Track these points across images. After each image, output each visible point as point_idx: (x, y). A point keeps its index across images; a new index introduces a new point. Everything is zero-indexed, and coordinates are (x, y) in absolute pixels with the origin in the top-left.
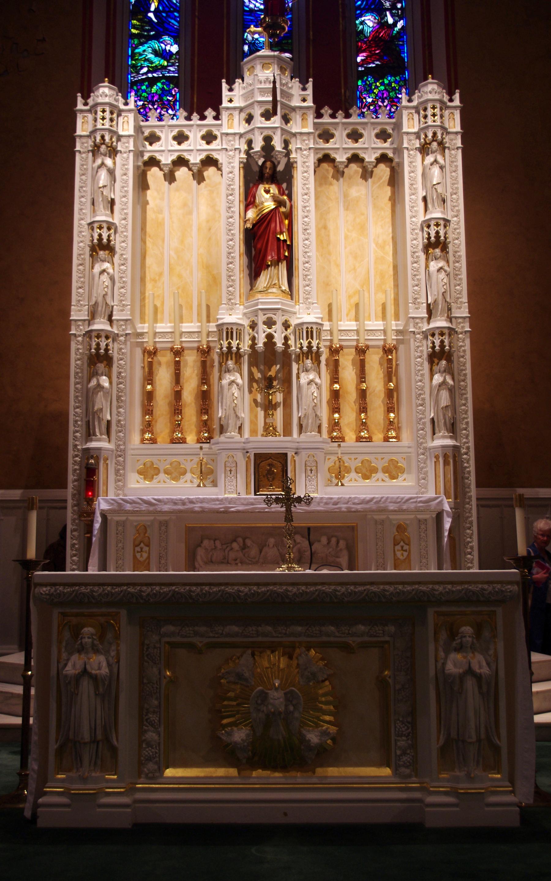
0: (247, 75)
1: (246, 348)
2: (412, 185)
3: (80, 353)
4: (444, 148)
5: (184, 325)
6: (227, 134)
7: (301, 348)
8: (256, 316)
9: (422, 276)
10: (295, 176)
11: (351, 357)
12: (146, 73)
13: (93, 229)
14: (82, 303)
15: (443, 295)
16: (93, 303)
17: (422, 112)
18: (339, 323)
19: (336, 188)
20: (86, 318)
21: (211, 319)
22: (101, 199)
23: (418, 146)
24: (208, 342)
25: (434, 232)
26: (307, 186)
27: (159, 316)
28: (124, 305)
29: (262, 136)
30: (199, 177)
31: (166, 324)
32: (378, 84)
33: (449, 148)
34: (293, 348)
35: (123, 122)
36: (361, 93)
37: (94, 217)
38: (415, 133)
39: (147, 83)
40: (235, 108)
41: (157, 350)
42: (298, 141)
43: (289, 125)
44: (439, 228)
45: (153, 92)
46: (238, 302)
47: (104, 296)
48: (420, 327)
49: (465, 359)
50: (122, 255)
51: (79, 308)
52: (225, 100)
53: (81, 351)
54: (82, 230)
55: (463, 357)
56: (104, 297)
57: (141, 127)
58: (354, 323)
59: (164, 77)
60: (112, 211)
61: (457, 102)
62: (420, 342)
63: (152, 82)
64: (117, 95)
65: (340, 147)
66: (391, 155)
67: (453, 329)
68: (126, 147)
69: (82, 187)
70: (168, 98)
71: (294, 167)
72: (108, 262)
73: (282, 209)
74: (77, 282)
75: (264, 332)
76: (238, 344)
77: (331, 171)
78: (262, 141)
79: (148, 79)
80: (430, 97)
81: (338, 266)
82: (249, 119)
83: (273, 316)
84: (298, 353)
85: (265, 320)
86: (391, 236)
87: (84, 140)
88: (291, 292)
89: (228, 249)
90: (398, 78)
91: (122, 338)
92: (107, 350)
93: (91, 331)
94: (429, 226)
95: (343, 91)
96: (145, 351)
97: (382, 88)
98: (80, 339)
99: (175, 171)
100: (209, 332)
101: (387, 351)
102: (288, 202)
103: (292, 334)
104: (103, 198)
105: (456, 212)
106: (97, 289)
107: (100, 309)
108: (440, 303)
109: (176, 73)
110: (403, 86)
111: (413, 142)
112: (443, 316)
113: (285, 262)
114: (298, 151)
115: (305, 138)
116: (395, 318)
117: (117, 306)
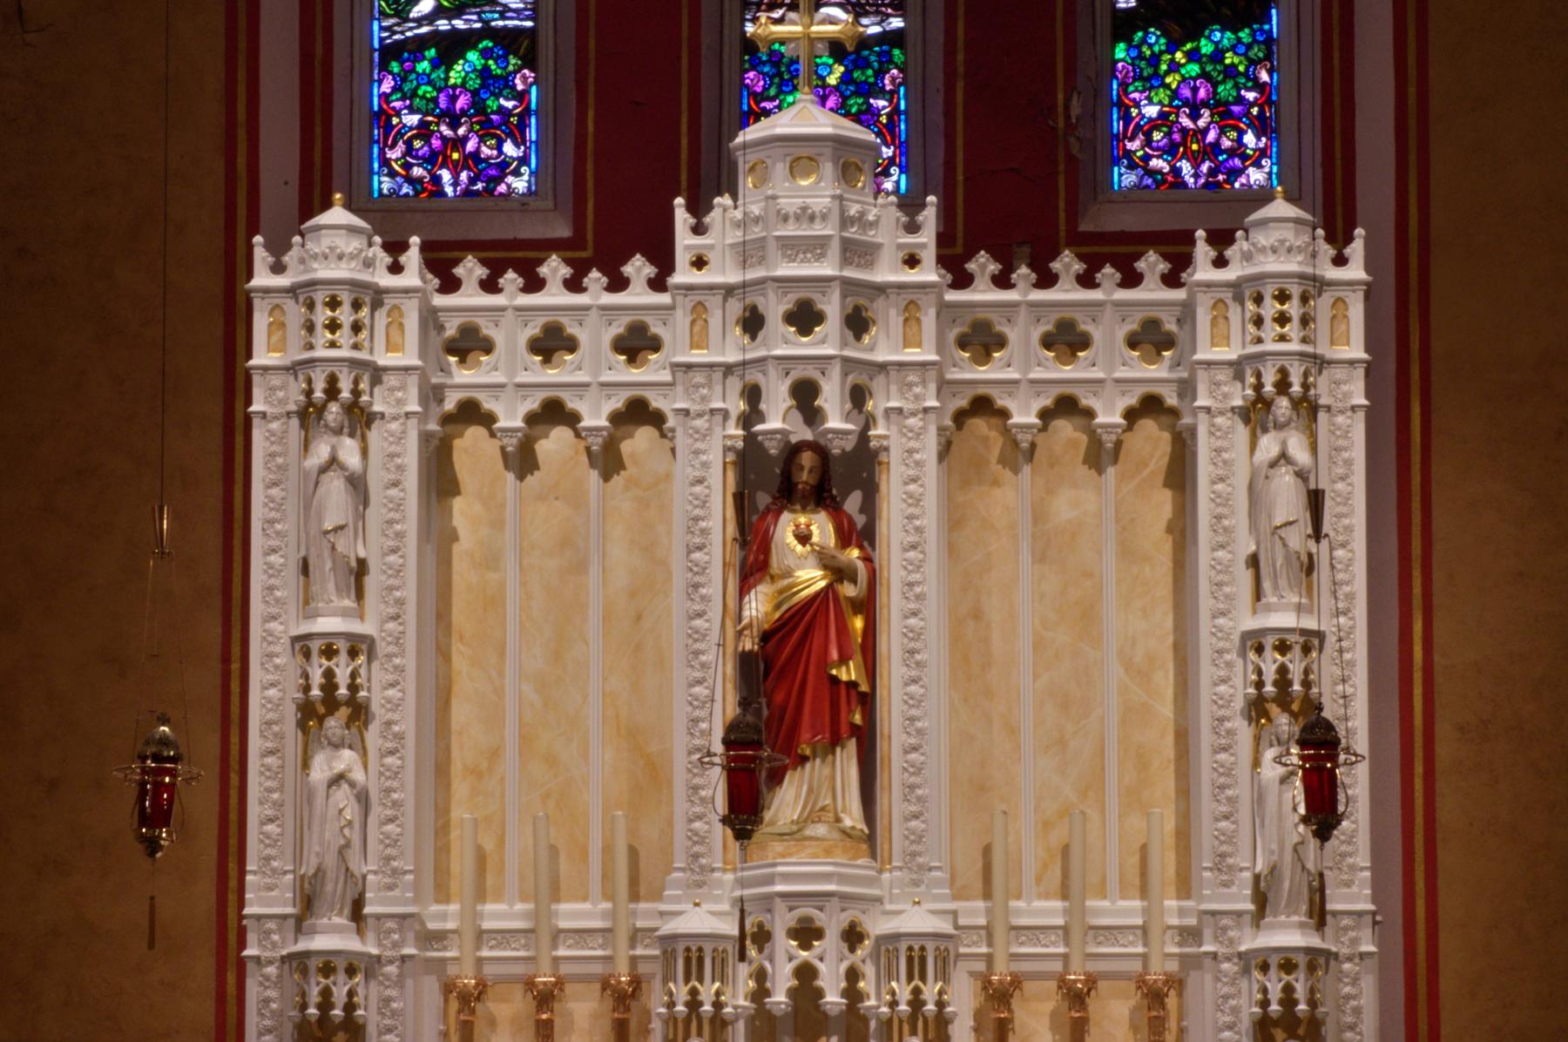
0: (747, 183)
1: (742, 1002)
2: (1219, 518)
3: (273, 1012)
4: (1314, 409)
5: (564, 907)
6: (689, 367)
7: (893, 1004)
8: (769, 911)
9: (1242, 791)
10: (883, 487)
11: (1049, 1006)
12: (430, 18)
13: (307, 654)
14: (275, 864)
15: (1295, 850)
16: (311, 872)
17: (1250, 306)
18: (1013, 904)
19: (1009, 496)
20: (290, 910)
21: (643, 890)
22: (329, 565)
23: (1238, 402)
24: (634, 961)
25: (1274, 667)
26: (918, 523)
27: (490, 881)
28: (395, 871)
29: (788, 382)
30: (608, 460)
31: (511, 904)
32: (1179, 55)
33: (1328, 408)
34: (872, 1002)
35: (389, 325)
36: (1124, 86)
37: (311, 616)
38: (1230, 364)
39: (431, 53)
40: (711, 288)
41: (485, 986)
42: (893, 388)
43: (866, 339)
44: (1289, 656)
45: (452, 81)
46: (719, 865)
47: (342, 851)
48: (1231, 942)
49: (1360, 1034)
50: (389, 723)
51: (269, 881)
52: (682, 258)
53: (274, 1006)
54: (272, 648)
55: (1352, 1028)
56: (340, 852)
57: (435, 311)
58: (1058, 904)
59: (488, 31)
60: (360, 595)
61: (1355, 271)
62: (1233, 984)
63: (452, 47)
64: (370, 245)
65: (1022, 375)
66: (1171, 400)
67: (1328, 954)
68: (396, 403)
69: (271, 522)
70: (502, 101)
71: (880, 463)
72: (350, 747)
73: (848, 590)
74: (261, 803)
75: (790, 959)
76: (718, 994)
77: (997, 442)
78: (786, 395)
79: (435, 38)
80: (1272, 265)
81: (1013, 731)
82: (753, 323)
83: (814, 913)
84: (884, 1018)
85: (793, 924)
86: (1171, 640)
87: (276, 380)
88: (870, 840)
89: (689, 709)
90: (1244, 35)
91: (392, 969)
92: (350, 1007)
93: (307, 954)
94: (1260, 650)
95: (1060, 96)
96: (448, 988)
97: (1194, 69)
98: (271, 970)
99: (536, 439)
100: (636, 931)
101: (1154, 997)
102: (860, 565)
103: (868, 961)
104: (334, 562)
105: (1343, 614)
106: (322, 831)
107: (329, 887)
108: (1287, 873)
109: (527, 18)
110: (1260, 61)
111: (1225, 389)
112: (1296, 912)
113: (852, 745)
114: (893, 417)
115: (912, 378)
116: (1178, 890)
117: (375, 873)
